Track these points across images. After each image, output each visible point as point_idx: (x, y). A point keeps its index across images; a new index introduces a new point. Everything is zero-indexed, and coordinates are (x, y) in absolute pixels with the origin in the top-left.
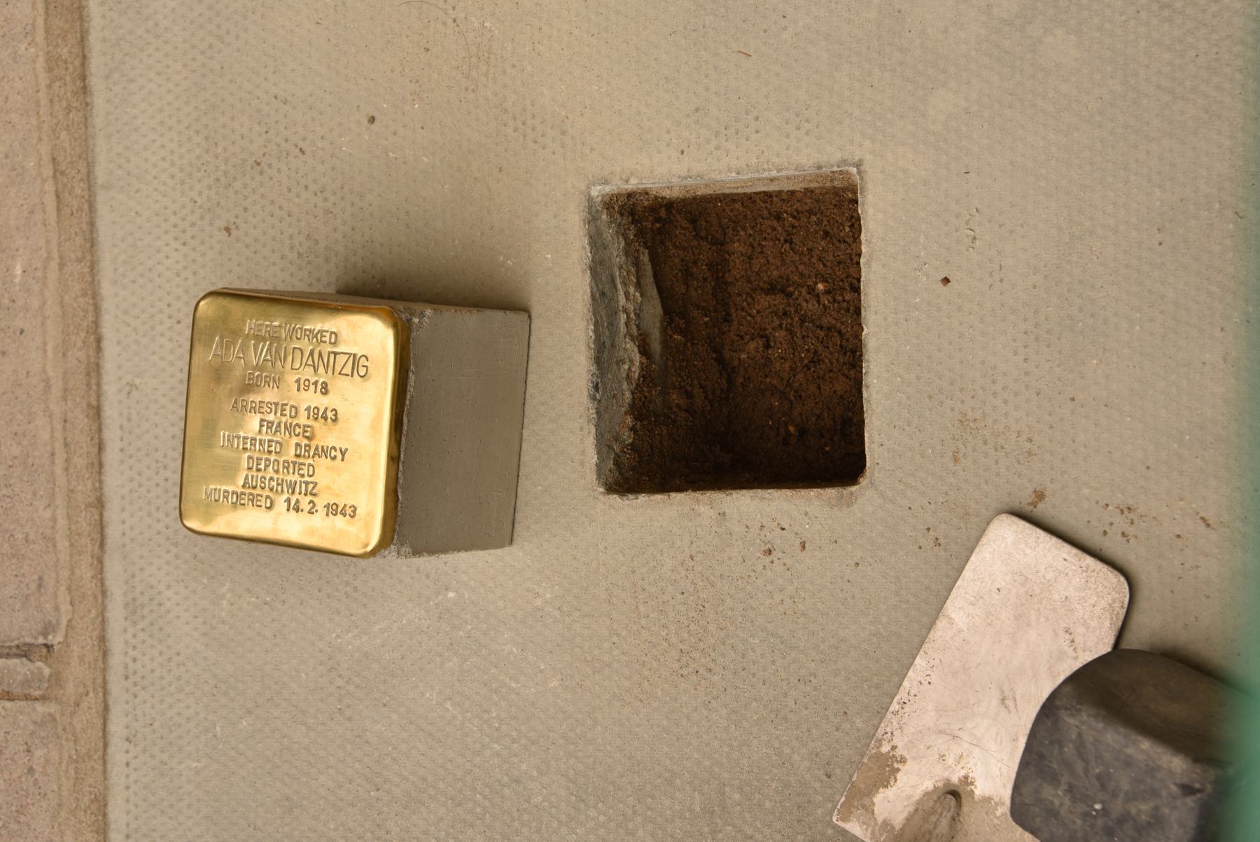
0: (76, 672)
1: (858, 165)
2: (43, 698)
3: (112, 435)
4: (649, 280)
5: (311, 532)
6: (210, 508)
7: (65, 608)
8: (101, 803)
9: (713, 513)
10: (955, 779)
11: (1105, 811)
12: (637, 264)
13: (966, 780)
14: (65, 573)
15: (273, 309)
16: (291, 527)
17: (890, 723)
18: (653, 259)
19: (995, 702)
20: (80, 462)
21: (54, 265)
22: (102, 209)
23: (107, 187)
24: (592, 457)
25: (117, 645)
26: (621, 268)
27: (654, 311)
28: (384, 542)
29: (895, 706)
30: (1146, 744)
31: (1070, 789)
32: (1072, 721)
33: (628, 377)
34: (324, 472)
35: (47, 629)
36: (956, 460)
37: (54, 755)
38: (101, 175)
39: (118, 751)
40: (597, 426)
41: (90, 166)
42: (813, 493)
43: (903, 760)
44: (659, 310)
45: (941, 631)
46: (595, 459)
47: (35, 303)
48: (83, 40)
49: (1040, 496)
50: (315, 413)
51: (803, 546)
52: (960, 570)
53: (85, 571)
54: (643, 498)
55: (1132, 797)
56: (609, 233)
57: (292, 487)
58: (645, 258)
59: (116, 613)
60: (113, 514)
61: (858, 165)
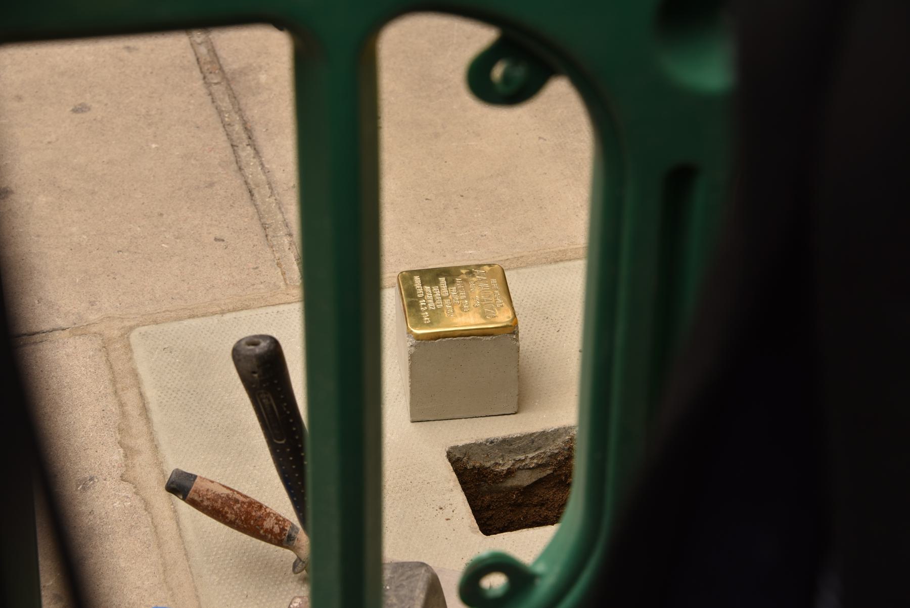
8: (247, 308)
9: (451, 487)
24: (461, 444)
26: (544, 453)
27: (524, 479)
30: (422, 596)
32: (423, 571)
33: (496, 464)
37: (262, 291)
38: (521, 271)
40: (474, 444)
41: (525, 267)
44: (526, 484)
55: (397, 596)
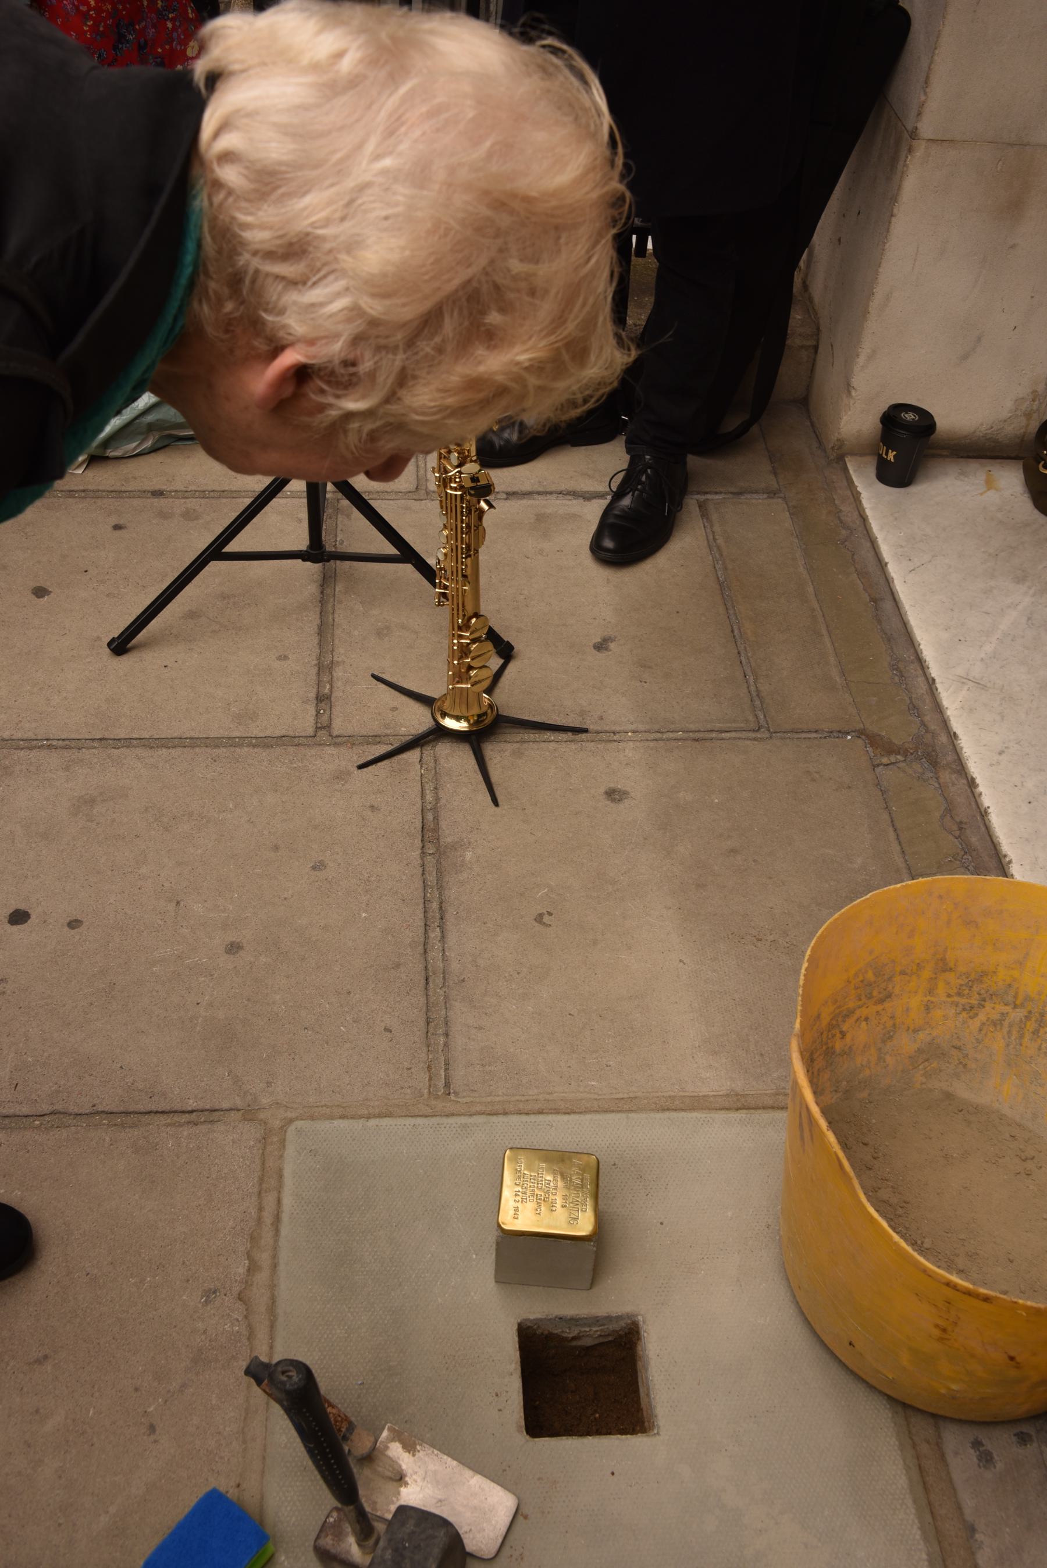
0: (439, 1105)
1: (658, 1434)
2: (429, 1092)
3: (532, 1118)
4: (602, 1340)
5: (507, 1200)
6: (514, 1160)
7: (465, 1100)
8: (390, 1115)
10: (407, 1479)
11: (405, 1548)
12: (609, 1335)
13: (406, 1484)
14: (478, 1100)
15: (594, 1185)
16: (507, 1193)
17: (429, 1450)
18: (610, 1342)
19: (439, 1497)
20: (521, 1106)
21: (596, 1096)
22: (619, 1115)
23: (627, 1118)
25: (451, 1120)
27: (588, 1342)
28: (503, 1230)
29: (436, 1452)
31: (413, 1532)
34: (530, 1205)
35: (456, 1094)
36: (539, 1479)
37: (408, 1097)
38: (632, 1115)
39: (409, 1121)
42: (522, 1414)
43: (414, 1455)
45: (468, 1473)
46: (532, 1318)
47: (581, 1090)
48: (682, 1110)
49: (526, 1517)
50: (554, 1202)
51: (500, 1410)
52: (493, 1481)
53: (479, 1108)
54: (517, 1339)
56: (622, 1324)
57: (525, 1193)
58: (610, 1338)
59: (463, 1120)
60: (501, 1118)
61: (658, 1434)
